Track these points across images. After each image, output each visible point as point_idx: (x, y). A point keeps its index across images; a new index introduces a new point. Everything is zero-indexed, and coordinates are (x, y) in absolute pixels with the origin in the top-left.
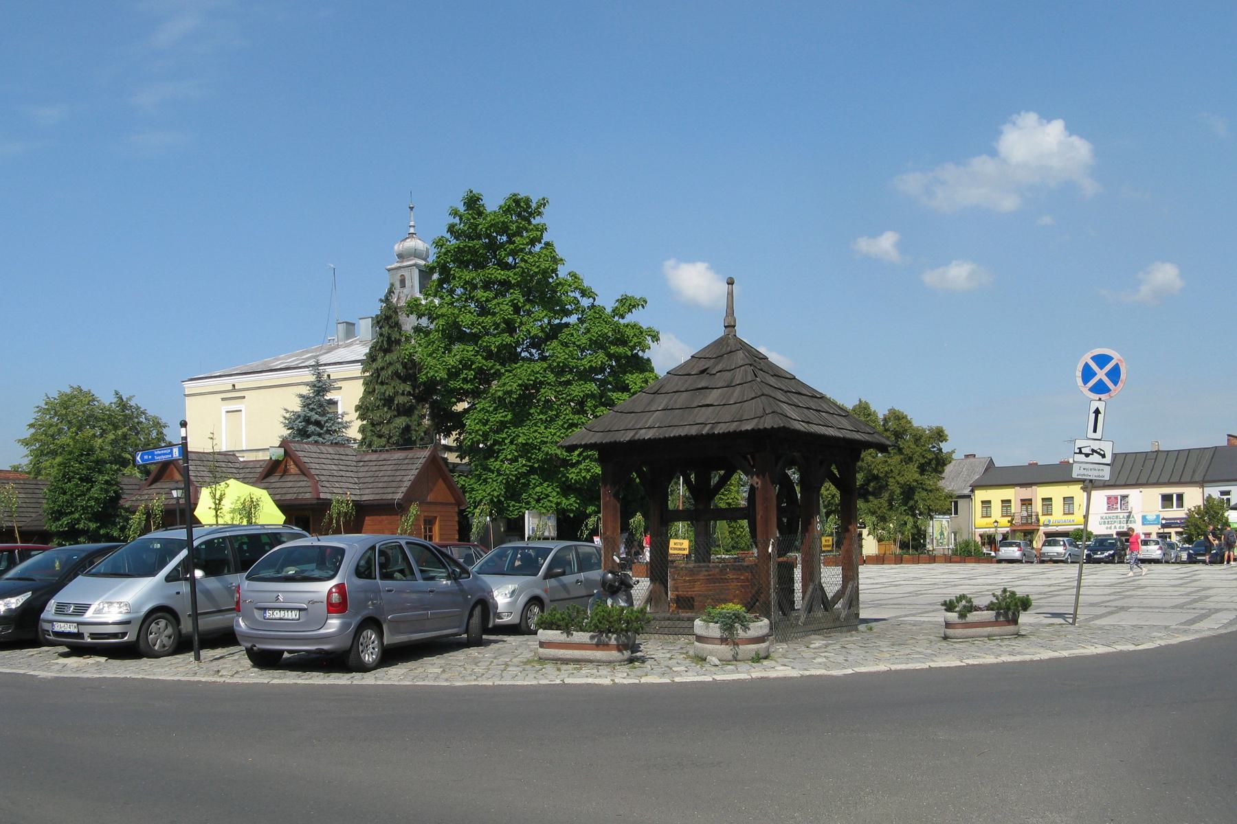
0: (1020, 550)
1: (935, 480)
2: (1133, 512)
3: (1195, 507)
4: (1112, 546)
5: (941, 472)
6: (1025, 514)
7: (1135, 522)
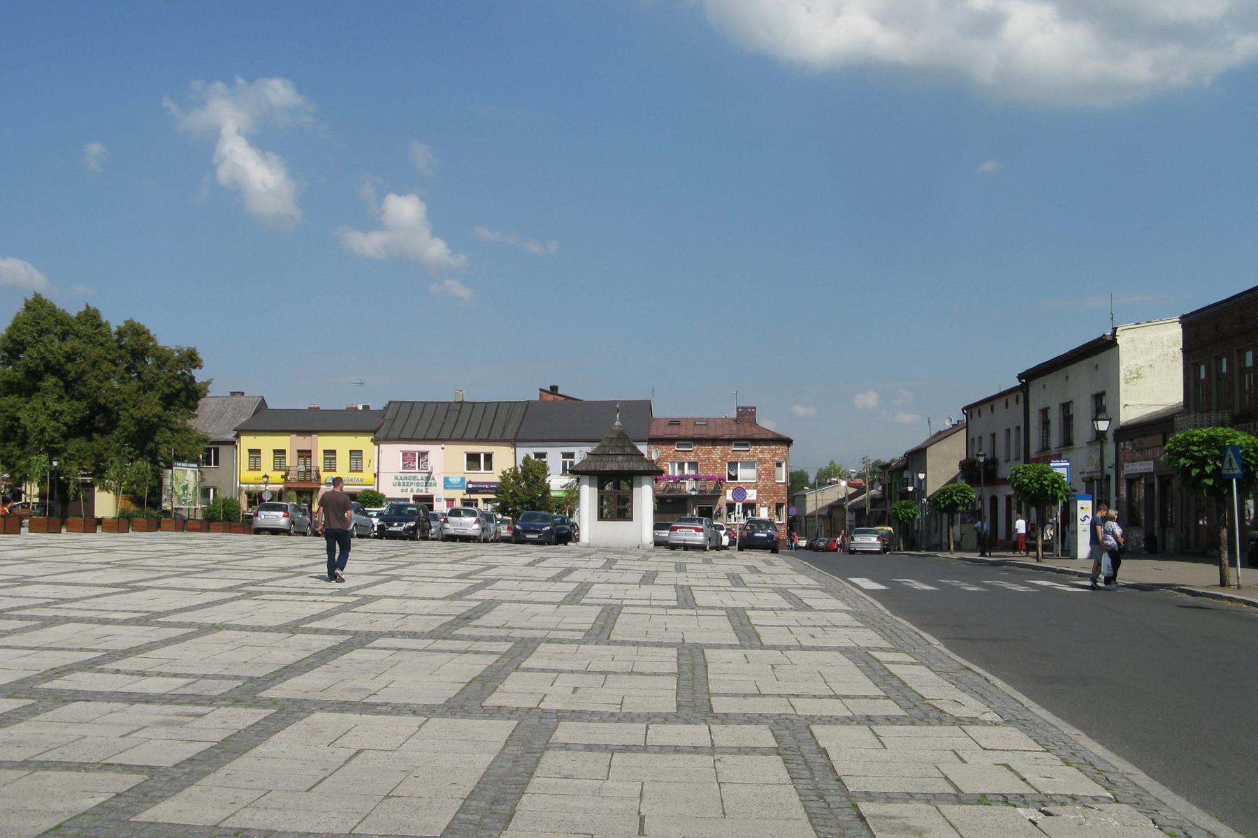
0: (288, 517)
1: (185, 417)
2: (434, 473)
3: (510, 470)
4: (411, 516)
5: (195, 408)
6: (302, 468)
7: (435, 485)
